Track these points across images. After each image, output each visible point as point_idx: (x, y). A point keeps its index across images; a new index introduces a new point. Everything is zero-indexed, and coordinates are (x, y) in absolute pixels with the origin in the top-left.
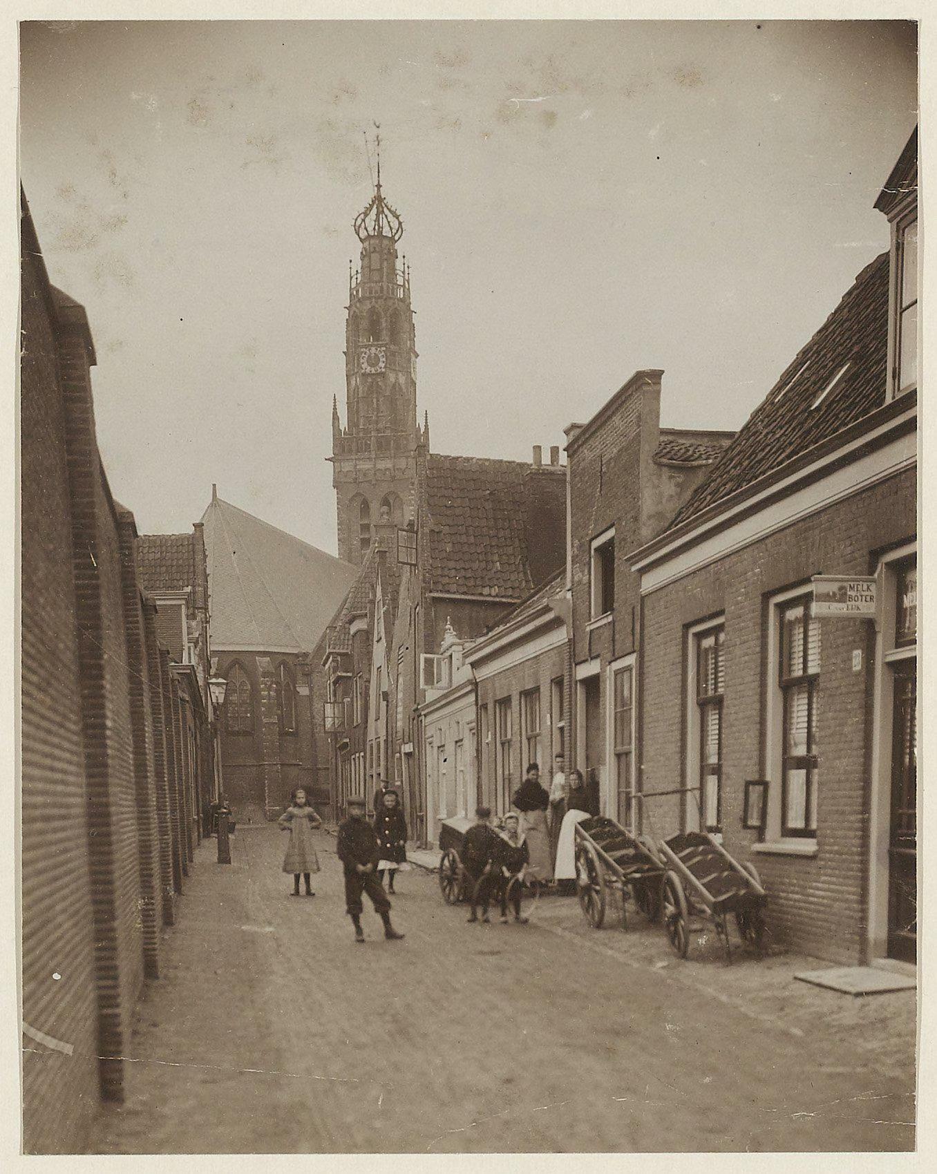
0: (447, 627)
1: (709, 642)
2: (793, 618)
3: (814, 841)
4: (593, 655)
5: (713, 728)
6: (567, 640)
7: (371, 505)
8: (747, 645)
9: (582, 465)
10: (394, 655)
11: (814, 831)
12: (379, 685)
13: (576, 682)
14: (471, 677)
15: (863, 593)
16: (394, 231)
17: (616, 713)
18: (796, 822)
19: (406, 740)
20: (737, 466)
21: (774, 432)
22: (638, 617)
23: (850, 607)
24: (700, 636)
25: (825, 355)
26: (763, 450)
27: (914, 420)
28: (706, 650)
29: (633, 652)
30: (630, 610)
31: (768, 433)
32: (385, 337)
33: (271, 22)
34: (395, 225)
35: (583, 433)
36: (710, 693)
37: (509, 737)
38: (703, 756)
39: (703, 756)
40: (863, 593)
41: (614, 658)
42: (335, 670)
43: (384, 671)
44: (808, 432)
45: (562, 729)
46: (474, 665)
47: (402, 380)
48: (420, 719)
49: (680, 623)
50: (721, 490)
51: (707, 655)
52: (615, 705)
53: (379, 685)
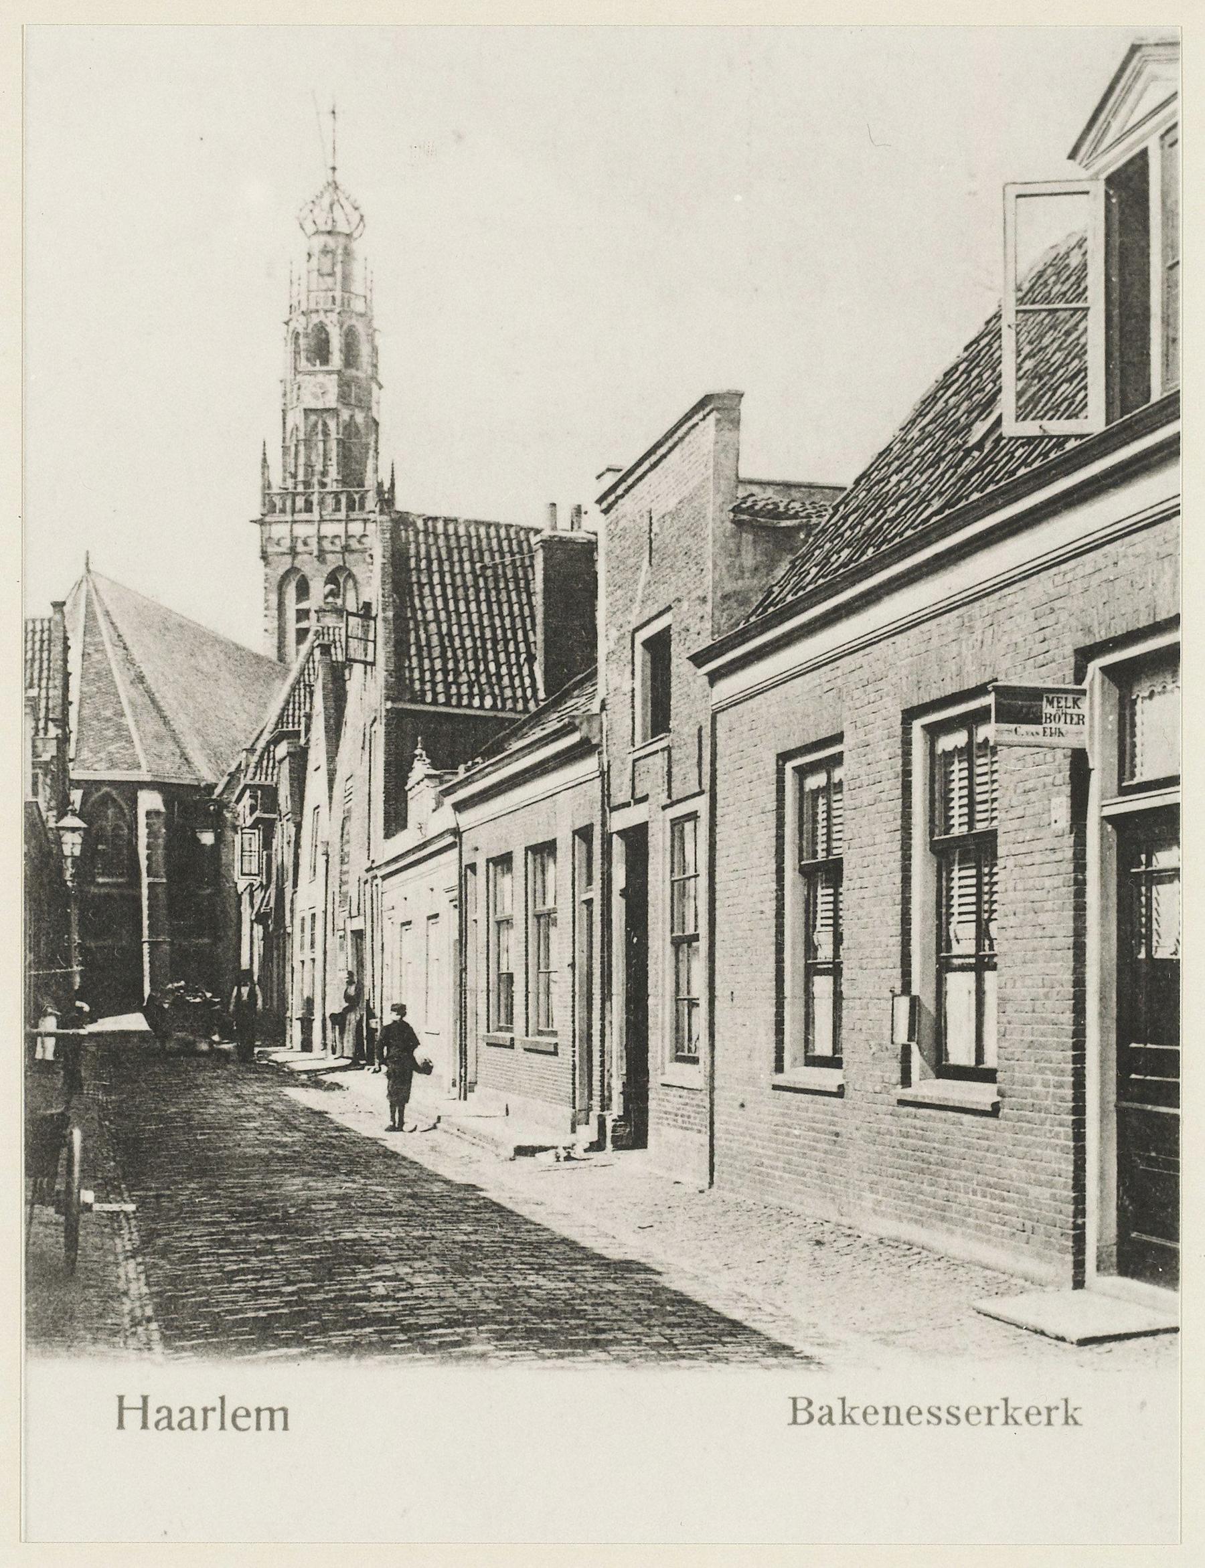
0: (418, 752)
1: (815, 781)
2: (950, 748)
3: (992, 1088)
4: (638, 796)
5: (823, 909)
6: (598, 774)
7: (312, 584)
8: (878, 787)
9: (623, 523)
10: (338, 792)
11: (994, 1071)
12: (315, 832)
13: (611, 834)
14: (453, 825)
15: (1069, 711)
16: (354, 226)
17: (673, 882)
18: (823, 1047)
19: (354, 913)
20: (856, 526)
21: (911, 479)
22: (707, 742)
23: (1048, 731)
24: (934, 732)
25: (980, 375)
26: (895, 503)
27: (1175, 439)
28: (948, 756)
29: (701, 793)
30: (696, 731)
31: (900, 482)
32: (336, 360)
33: (29, 1098)
34: (355, 218)
35: (623, 480)
36: (821, 856)
37: (550, 904)
38: (810, 947)
39: (810, 947)
40: (1069, 711)
41: (669, 801)
42: (253, 809)
43: (324, 810)
44: (967, 477)
45: (589, 902)
46: (459, 807)
47: (360, 418)
48: (376, 882)
49: (899, 709)
50: (833, 559)
51: (815, 800)
52: (672, 871)
53: (315, 832)
